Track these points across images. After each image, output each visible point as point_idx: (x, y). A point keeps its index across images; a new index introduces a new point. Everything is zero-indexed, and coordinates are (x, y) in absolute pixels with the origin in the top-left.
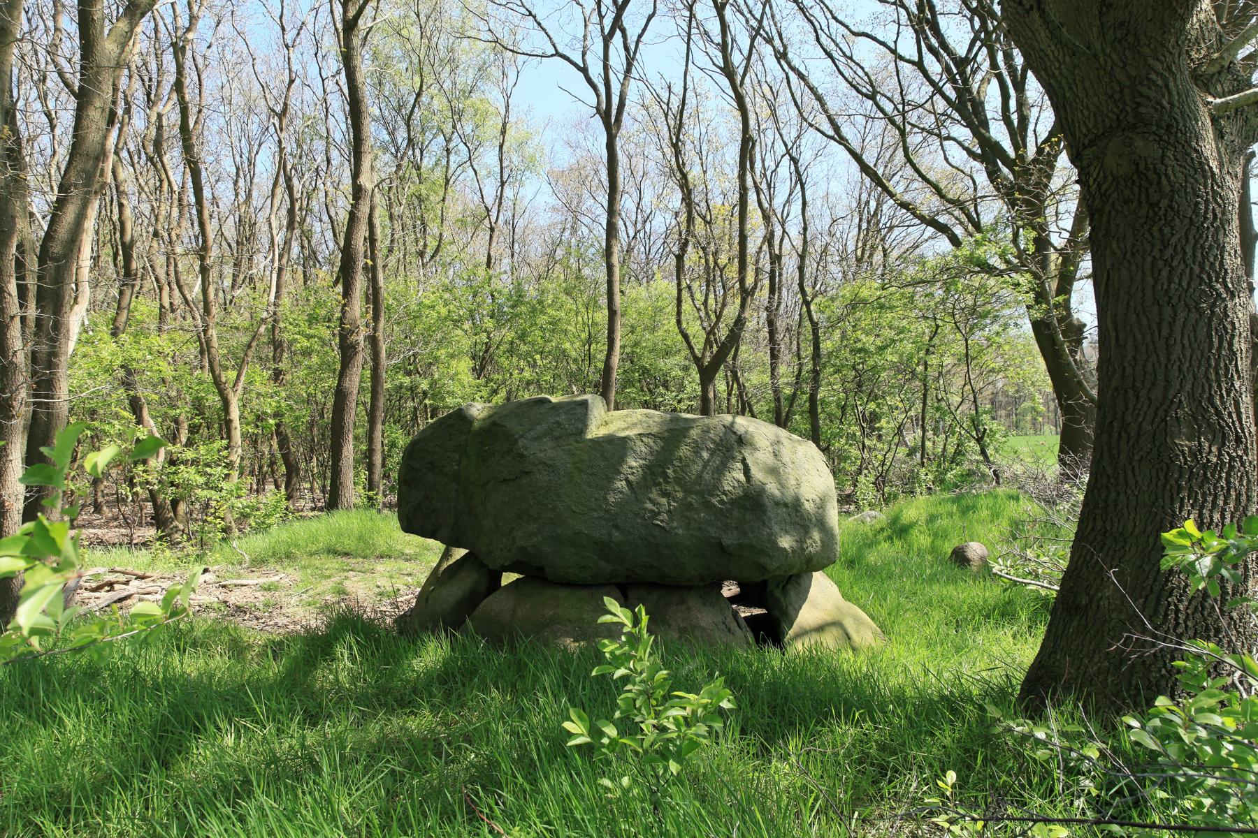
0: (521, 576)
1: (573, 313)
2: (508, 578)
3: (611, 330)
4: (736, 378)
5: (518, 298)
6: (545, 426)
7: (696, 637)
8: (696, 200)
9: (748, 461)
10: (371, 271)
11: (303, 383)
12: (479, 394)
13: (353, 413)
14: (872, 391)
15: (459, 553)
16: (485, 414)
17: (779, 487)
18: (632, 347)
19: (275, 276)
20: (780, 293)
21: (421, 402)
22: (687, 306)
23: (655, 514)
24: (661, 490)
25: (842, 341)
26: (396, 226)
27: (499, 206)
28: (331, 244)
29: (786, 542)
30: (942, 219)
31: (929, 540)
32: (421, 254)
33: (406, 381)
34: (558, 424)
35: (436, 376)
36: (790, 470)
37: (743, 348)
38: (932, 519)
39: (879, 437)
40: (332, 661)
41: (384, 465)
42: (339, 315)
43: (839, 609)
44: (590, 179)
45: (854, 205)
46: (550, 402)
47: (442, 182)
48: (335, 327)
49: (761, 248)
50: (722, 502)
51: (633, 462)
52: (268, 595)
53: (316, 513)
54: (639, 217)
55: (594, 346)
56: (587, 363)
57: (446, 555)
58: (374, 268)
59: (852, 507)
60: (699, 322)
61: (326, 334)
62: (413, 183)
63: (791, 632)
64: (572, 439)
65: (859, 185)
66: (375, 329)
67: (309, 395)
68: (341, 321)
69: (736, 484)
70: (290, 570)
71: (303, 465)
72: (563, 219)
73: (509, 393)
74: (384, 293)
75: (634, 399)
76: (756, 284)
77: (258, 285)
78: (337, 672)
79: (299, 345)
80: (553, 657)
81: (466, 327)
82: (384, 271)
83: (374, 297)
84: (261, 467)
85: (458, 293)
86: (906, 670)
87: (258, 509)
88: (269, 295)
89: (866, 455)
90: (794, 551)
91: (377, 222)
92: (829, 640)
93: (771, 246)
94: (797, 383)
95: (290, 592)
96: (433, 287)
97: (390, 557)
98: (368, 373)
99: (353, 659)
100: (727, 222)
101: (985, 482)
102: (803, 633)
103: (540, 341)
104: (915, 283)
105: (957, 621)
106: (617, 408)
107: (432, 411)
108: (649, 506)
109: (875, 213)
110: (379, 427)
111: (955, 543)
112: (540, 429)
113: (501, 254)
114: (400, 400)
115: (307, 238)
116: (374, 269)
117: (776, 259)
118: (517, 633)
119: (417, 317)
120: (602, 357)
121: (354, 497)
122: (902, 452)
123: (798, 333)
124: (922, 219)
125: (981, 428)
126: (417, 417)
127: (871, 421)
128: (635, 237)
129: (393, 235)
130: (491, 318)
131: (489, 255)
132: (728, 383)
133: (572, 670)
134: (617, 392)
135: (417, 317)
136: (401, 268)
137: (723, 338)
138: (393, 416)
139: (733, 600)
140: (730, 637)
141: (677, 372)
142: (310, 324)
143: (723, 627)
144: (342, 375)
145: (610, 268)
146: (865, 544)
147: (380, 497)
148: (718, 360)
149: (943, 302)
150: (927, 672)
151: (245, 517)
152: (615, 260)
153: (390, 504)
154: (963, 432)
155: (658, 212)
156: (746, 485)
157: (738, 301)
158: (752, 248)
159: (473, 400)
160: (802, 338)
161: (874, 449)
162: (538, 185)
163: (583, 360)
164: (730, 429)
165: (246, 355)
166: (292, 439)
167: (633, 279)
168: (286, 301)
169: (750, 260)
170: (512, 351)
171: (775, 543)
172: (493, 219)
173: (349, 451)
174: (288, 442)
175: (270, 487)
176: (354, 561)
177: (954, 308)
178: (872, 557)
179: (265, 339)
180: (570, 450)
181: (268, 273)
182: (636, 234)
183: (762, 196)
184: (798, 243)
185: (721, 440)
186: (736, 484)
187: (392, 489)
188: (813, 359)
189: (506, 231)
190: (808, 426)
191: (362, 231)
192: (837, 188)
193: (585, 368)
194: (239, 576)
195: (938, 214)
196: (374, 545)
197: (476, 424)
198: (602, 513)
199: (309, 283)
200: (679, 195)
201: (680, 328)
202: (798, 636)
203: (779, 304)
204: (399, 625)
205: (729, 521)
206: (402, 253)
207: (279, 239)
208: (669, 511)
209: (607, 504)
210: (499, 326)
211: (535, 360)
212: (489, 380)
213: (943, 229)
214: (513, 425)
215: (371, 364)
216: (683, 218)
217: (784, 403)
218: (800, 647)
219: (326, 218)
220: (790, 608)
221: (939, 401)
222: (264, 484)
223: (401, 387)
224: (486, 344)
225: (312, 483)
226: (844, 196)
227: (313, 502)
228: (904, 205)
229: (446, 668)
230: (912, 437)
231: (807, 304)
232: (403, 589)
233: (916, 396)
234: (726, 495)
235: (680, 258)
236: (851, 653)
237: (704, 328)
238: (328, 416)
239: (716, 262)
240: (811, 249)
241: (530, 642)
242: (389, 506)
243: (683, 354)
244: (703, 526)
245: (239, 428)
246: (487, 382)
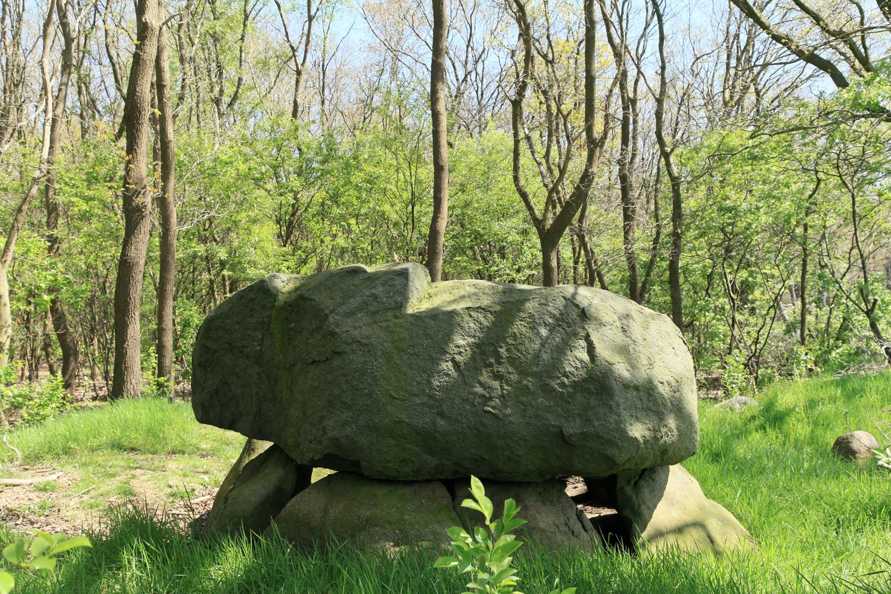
0: (333, 472)
1: (392, 170)
2: (319, 474)
3: (438, 189)
4: (583, 244)
5: (329, 152)
6: (359, 299)
7: (534, 541)
8: (536, 36)
9: (592, 338)
10: (160, 123)
11: (81, 253)
12: (286, 264)
13: (139, 287)
14: (743, 256)
15: (263, 446)
16: (291, 286)
17: (629, 368)
18: (462, 208)
19: (48, 128)
20: (634, 143)
21: (218, 274)
22: (525, 160)
23: (486, 400)
24: (493, 372)
25: (707, 200)
26: (187, 69)
27: (307, 45)
28: (113, 91)
29: (638, 431)
30: (825, 54)
31: (809, 429)
32: (217, 102)
33: (201, 249)
34: (375, 297)
35: (236, 244)
36: (641, 348)
37: (591, 208)
38: (811, 404)
39: (752, 311)
40: (118, 569)
41: (176, 347)
42: (123, 173)
43: (702, 508)
44: (411, 12)
45: (721, 38)
46: (365, 272)
47: (241, 18)
48: (119, 187)
49: (611, 91)
50: (563, 385)
51: (461, 341)
52: (44, 496)
53: (97, 403)
54: (470, 56)
55: (417, 208)
56: (410, 227)
57: (248, 449)
58: (163, 119)
59: (720, 393)
60: (539, 179)
61: (108, 196)
62: (208, 19)
63: (644, 535)
64: (390, 314)
65: (727, 15)
66: (164, 189)
67: (89, 266)
68: (125, 180)
69: (579, 365)
70: (69, 468)
71: (81, 347)
72: (382, 59)
73: (321, 263)
74: (174, 148)
75: (465, 268)
76: (605, 133)
77: (28, 139)
78: (124, 580)
79: (76, 209)
80: (369, 562)
81: (269, 186)
82: (174, 122)
83: (163, 152)
84: (33, 350)
85: (259, 147)
86: (776, 577)
87: (31, 399)
88: (41, 150)
89: (736, 331)
90: (646, 442)
91: (166, 65)
92: (689, 542)
93: (623, 88)
94: (654, 248)
95: (69, 493)
96: (231, 140)
97: (184, 453)
98: (157, 241)
99: (142, 566)
100: (572, 61)
101: (876, 361)
102: (659, 534)
103: (355, 202)
104: (790, 130)
105: (838, 522)
106: (445, 277)
107: (231, 284)
108: (479, 390)
109: (746, 49)
110: (170, 303)
111: (839, 431)
112: (353, 303)
113: (310, 102)
114: (193, 272)
115: (85, 84)
116: (163, 119)
117: (629, 103)
118: (328, 536)
119: (214, 175)
120: (427, 220)
121: (141, 385)
122: (779, 328)
123: (656, 190)
124: (800, 54)
125: (871, 298)
126: (213, 291)
127: (743, 292)
128: (465, 80)
129: (184, 80)
130: (299, 175)
131: (295, 102)
132: (574, 249)
133: (392, 577)
134: (445, 262)
135: (214, 175)
136: (194, 119)
137: (568, 197)
138: (186, 289)
139: (577, 499)
140: (574, 540)
141: (514, 237)
142: (90, 183)
143: (566, 529)
144: (126, 243)
145: (436, 116)
146: (733, 435)
147: (171, 384)
148: (562, 222)
149: (826, 151)
150: (800, 577)
151: (16, 407)
152: (441, 107)
153: (183, 392)
154: (850, 304)
155: (491, 50)
156: (590, 365)
157: (585, 154)
158: (600, 91)
159: (279, 271)
160: (660, 195)
161: (747, 325)
162: (352, 20)
163: (406, 224)
164: (571, 301)
165: (16, 220)
166: (69, 317)
167: (463, 128)
168: (60, 157)
169: (598, 104)
170: (323, 213)
171: (624, 432)
172: (300, 60)
173: (135, 331)
174: (65, 321)
175: (44, 373)
176: (142, 457)
177: (838, 159)
178: (741, 450)
179: (36, 203)
180: (388, 327)
181: (39, 125)
182: (466, 76)
183: (612, 30)
184: (655, 84)
185: (561, 314)
186: (579, 365)
187: (185, 375)
188: (673, 220)
189: (315, 74)
190: (668, 298)
191: (148, 77)
192: (700, 19)
193: (408, 233)
194: (11, 475)
195: (816, 49)
196: (165, 439)
197: (281, 298)
198: (425, 399)
199: (87, 136)
200: (517, 31)
201: (517, 185)
202: (653, 538)
203: (634, 156)
204: (194, 531)
205: (571, 407)
206: (195, 100)
207: (53, 84)
208: (503, 396)
209: (431, 388)
210: (308, 185)
211: (349, 225)
212: (296, 248)
213: (825, 66)
214: (322, 299)
215: (160, 230)
216: (520, 56)
217: (640, 271)
218: (653, 550)
219: (106, 61)
220: (643, 507)
221: (822, 267)
222: (37, 370)
223: (195, 256)
224: (293, 205)
225: (92, 368)
226: (709, 28)
227: (94, 390)
228: (777, 38)
229: (248, 577)
230: (791, 310)
231: (666, 155)
232: (199, 489)
233: (795, 261)
234: (567, 377)
235: (517, 104)
236: (712, 557)
237: (546, 186)
238: (111, 293)
239: (559, 110)
240: (671, 92)
241: (344, 547)
242: (182, 395)
243: (521, 215)
244: (540, 413)
245: (8, 305)
246: (294, 251)
